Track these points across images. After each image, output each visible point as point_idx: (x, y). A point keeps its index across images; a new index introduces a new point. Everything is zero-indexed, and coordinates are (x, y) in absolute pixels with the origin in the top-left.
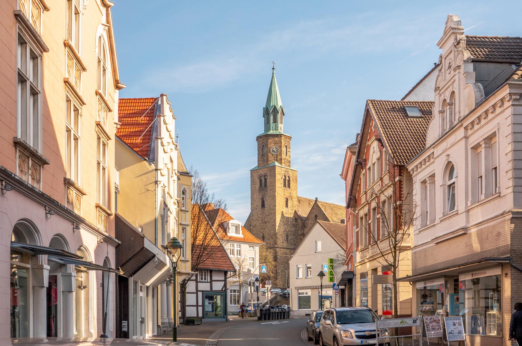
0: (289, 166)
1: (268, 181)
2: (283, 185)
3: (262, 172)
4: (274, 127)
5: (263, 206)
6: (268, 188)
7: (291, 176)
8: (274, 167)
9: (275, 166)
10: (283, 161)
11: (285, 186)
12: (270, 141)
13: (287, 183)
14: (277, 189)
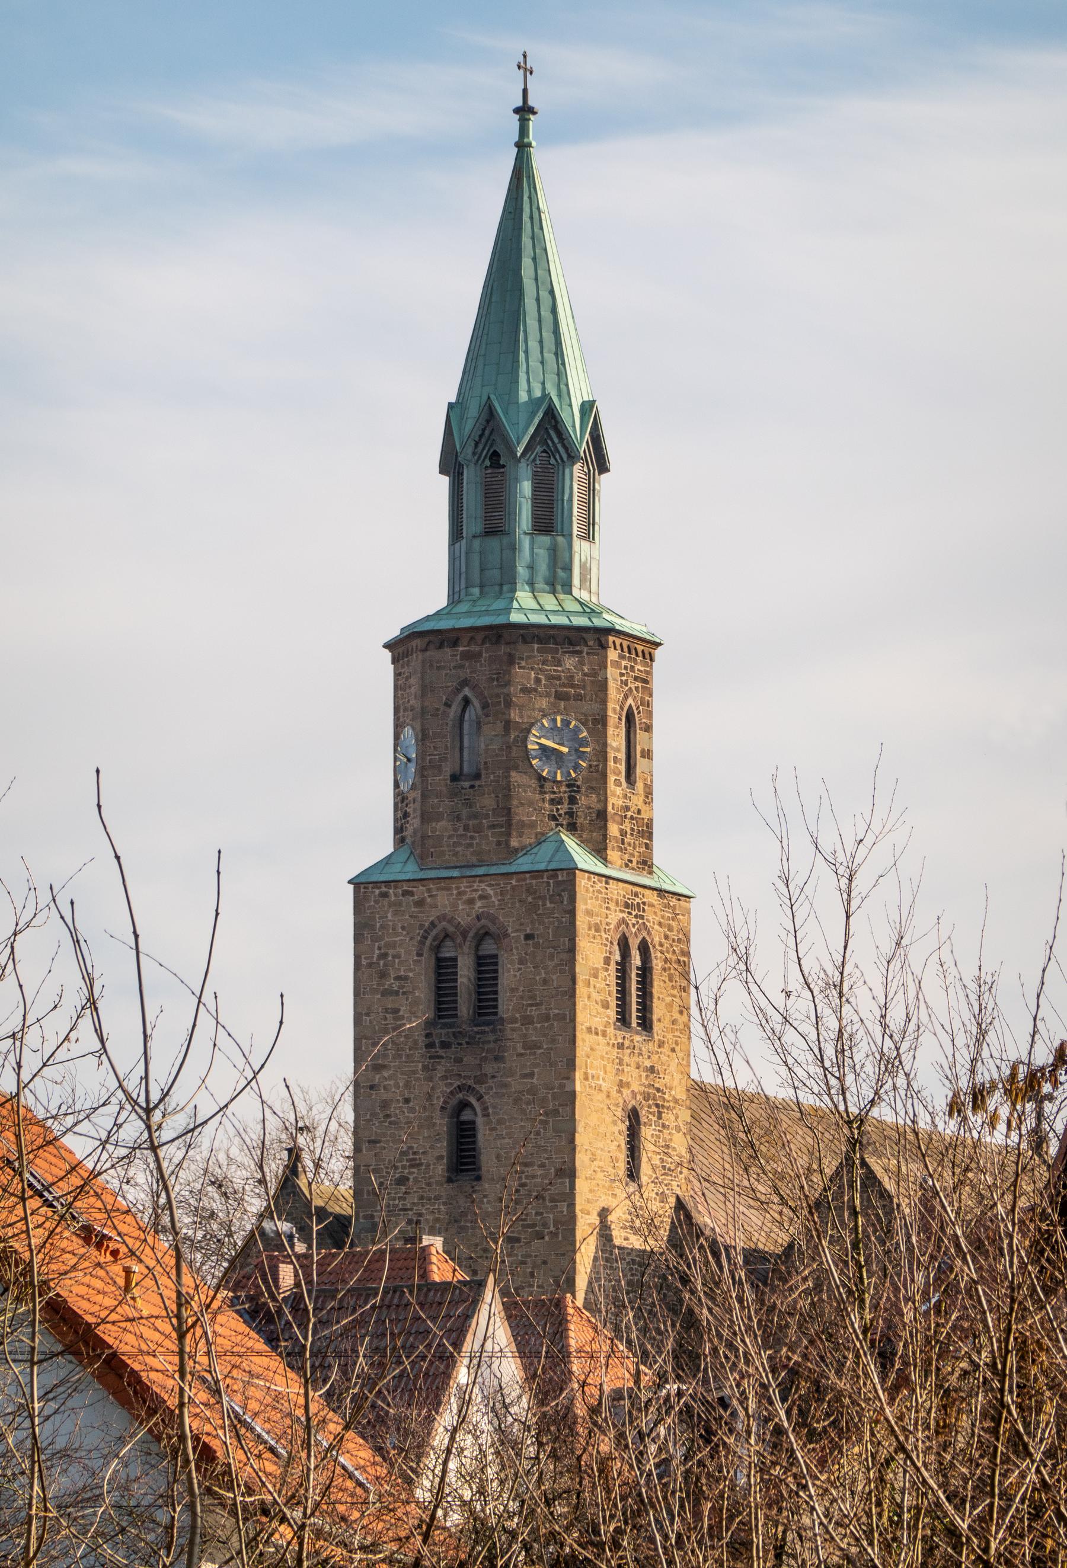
0: (646, 865)
1: (509, 976)
2: (612, 1013)
3: (459, 905)
4: (543, 567)
5: (464, 1159)
6: (514, 1037)
7: (656, 937)
8: (564, 879)
9: (572, 871)
10: (613, 829)
11: (623, 1019)
12: (524, 675)
13: (635, 1009)
14: (584, 1042)
